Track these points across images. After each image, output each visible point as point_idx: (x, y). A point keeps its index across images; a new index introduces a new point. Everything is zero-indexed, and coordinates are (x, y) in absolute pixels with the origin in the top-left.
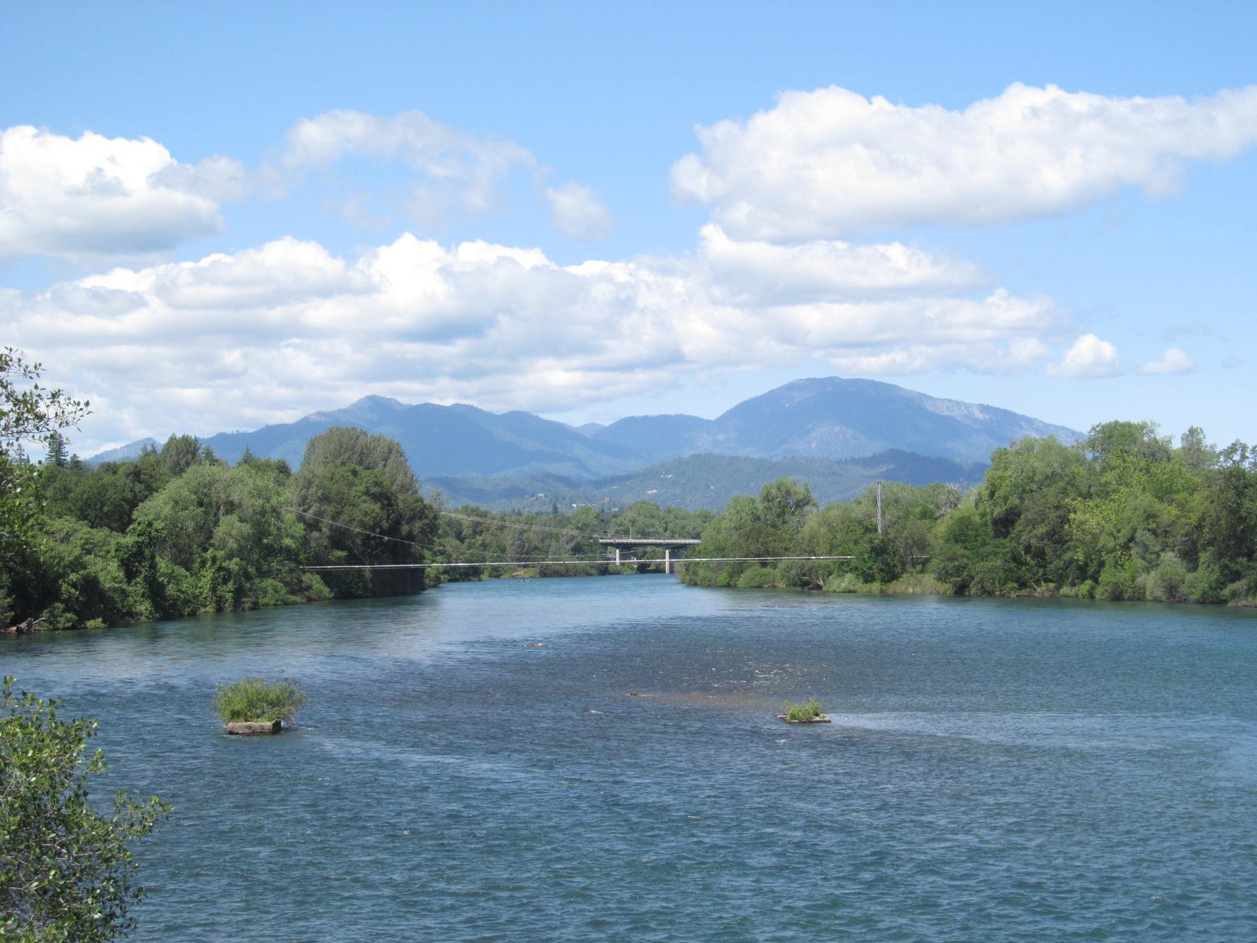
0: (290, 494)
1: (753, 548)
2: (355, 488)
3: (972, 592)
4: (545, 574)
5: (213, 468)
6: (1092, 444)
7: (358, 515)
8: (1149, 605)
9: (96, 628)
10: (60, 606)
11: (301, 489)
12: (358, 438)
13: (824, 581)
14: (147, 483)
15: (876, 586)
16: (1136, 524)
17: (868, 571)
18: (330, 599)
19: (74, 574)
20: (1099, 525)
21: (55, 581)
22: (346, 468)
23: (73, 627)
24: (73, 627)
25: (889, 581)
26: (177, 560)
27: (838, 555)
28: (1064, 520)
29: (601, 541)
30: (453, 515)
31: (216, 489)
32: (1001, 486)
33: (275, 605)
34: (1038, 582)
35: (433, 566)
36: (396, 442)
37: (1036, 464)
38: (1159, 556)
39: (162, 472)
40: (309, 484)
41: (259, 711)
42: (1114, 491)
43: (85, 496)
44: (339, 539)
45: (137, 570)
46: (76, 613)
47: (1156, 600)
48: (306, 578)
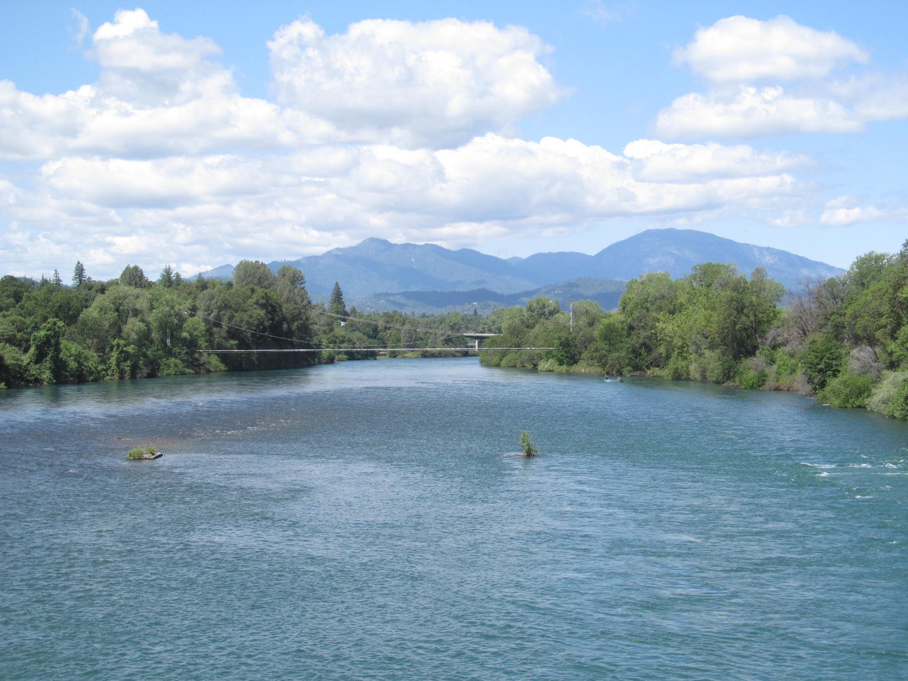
4: (425, 355)
15: (564, 368)
25: (572, 365)
33: (175, 374)
44: (233, 334)
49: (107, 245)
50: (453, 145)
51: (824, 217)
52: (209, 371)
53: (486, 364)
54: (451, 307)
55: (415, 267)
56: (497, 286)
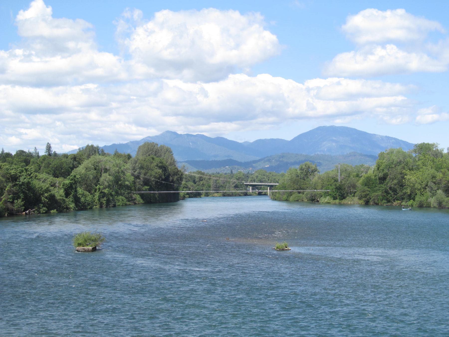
0: (129, 166)
1: (295, 187)
2: (153, 164)
3: (371, 204)
4: (224, 195)
5: (100, 156)
6: (415, 151)
7: (153, 173)
8: (432, 209)
9: (54, 213)
10: (42, 205)
11: (133, 164)
12: (154, 146)
13: (320, 199)
14: (78, 161)
15: (337, 201)
16: (428, 180)
17: (335, 195)
18: (143, 203)
19: (46, 194)
20: (415, 180)
21: (40, 197)
22: (150, 157)
23: (46, 213)
24: (46, 213)
25: (342, 199)
26: (86, 189)
27: (324, 190)
28: (403, 178)
29: (245, 184)
30: (192, 174)
31: (101, 164)
32: (381, 165)
33: (122, 205)
34: (394, 200)
35: (182, 192)
36: (169, 148)
37: (394, 158)
38: (436, 192)
39: (84, 157)
40: (136, 162)
41: (88, 243)
42: (421, 168)
43: (55, 166)
44: (146, 182)
45: (70, 192)
46: (47, 207)
47: (434, 207)
48: (134, 196)
49: (19, 135)
50: (216, 80)
51: (418, 118)
52: (135, 204)
53: (275, 199)
54: (214, 169)
55: (192, 147)
56: (237, 157)
